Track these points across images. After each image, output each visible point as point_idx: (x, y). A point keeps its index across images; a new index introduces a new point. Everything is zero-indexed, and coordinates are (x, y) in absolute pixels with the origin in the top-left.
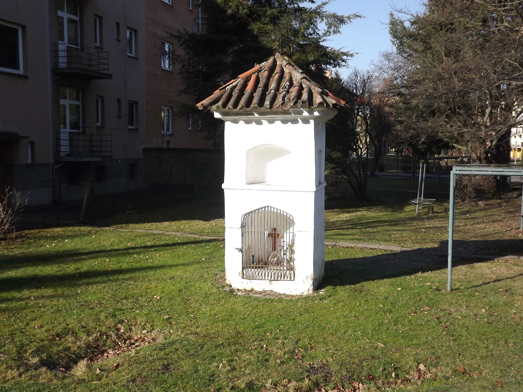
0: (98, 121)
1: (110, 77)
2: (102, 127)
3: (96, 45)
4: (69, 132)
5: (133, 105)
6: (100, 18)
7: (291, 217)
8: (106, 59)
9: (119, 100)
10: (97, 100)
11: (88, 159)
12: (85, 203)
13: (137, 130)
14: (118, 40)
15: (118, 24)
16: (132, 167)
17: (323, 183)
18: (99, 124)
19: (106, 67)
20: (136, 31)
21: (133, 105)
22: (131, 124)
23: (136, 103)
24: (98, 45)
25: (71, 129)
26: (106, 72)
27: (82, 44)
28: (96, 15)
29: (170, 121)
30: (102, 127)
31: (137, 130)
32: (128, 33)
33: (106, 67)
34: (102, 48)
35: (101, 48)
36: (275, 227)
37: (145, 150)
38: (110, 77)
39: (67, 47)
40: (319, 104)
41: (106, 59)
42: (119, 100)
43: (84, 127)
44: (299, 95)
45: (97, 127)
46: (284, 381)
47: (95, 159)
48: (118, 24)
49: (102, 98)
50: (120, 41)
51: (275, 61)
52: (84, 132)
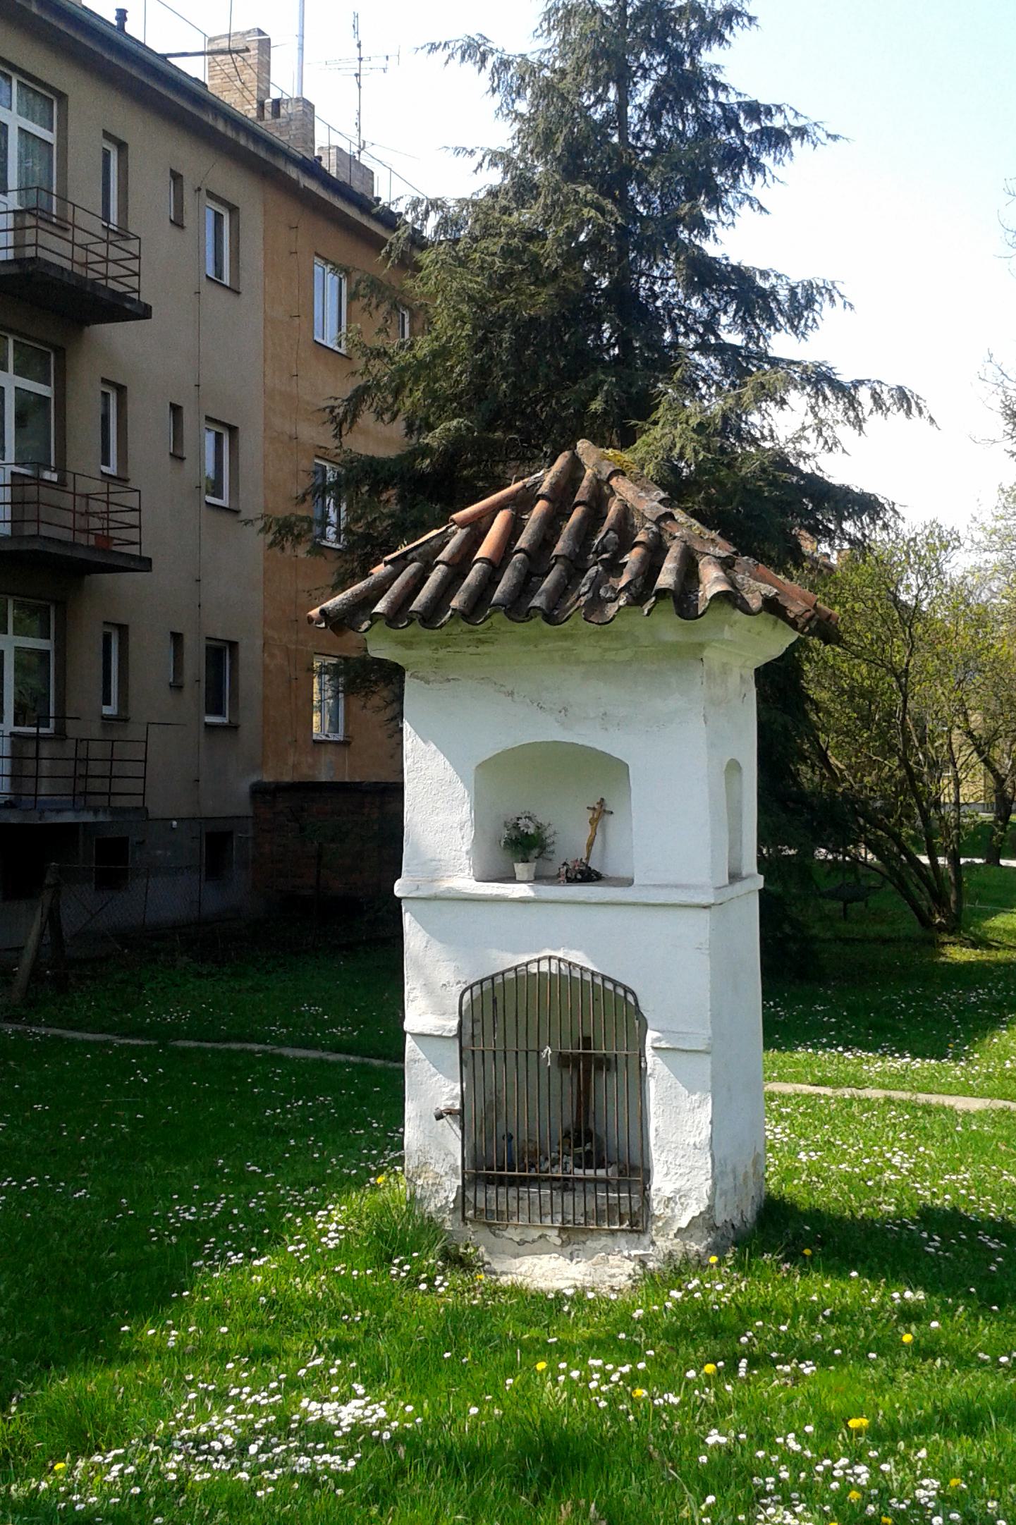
0: (107, 701)
1: (144, 564)
2: (122, 719)
3: (105, 469)
4: (12, 734)
5: (221, 654)
6: (121, 390)
7: (630, 998)
8: (133, 510)
9: (177, 638)
10: (107, 639)
11: (68, 818)
12: (27, 959)
13: (232, 728)
14: (177, 457)
15: (176, 409)
16: (217, 843)
17: (749, 876)
18: (108, 710)
19: (132, 535)
20: (233, 430)
21: (221, 654)
22: (219, 711)
23: (233, 645)
24: (112, 470)
25: (15, 725)
26: (134, 550)
27: (61, 469)
28: (105, 381)
29: (342, 703)
30: (122, 719)
31: (232, 728)
32: (209, 439)
33: (132, 535)
34: (127, 480)
35: (121, 480)
36: (586, 1034)
37: (260, 792)
38: (144, 564)
39: (13, 474)
40: (712, 598)
41: (133, 510)
42: (177, 638)
43: (61, 717)
44: (651, 568)
45: (105, 718)
46: (807, 1371)
47: (88, 818)
48: (176, 409)
49: (123, 629)
50: (182, 459)
51: (576, 465)
52: (60, 735)
